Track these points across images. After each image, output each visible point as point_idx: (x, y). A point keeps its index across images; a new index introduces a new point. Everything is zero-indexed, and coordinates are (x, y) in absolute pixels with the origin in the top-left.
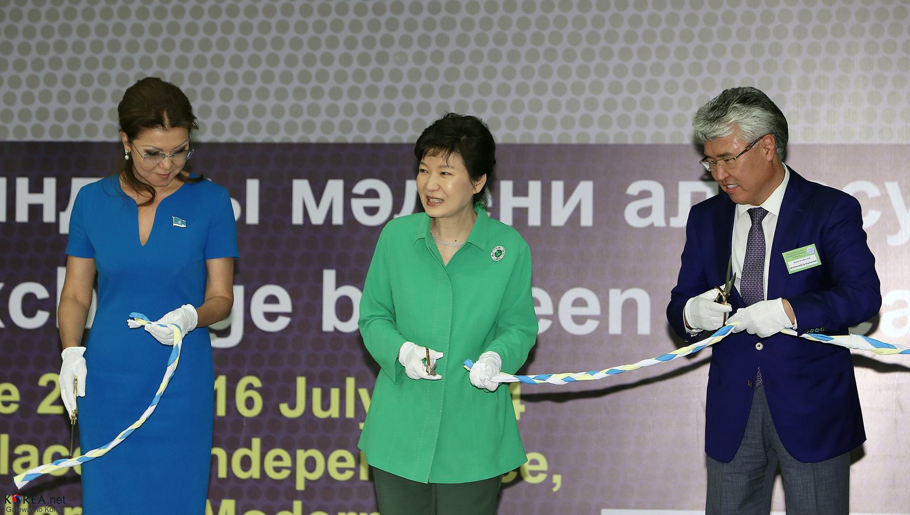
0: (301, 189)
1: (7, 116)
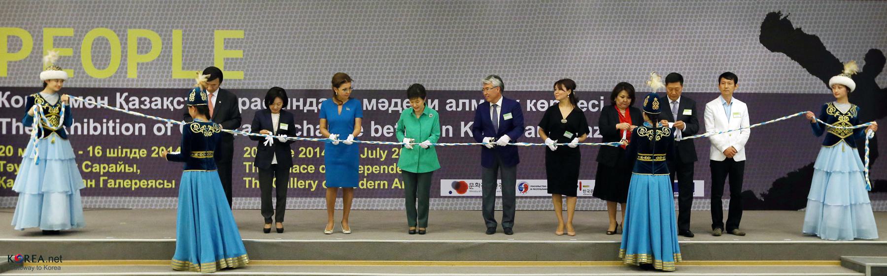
0: (365, 101)
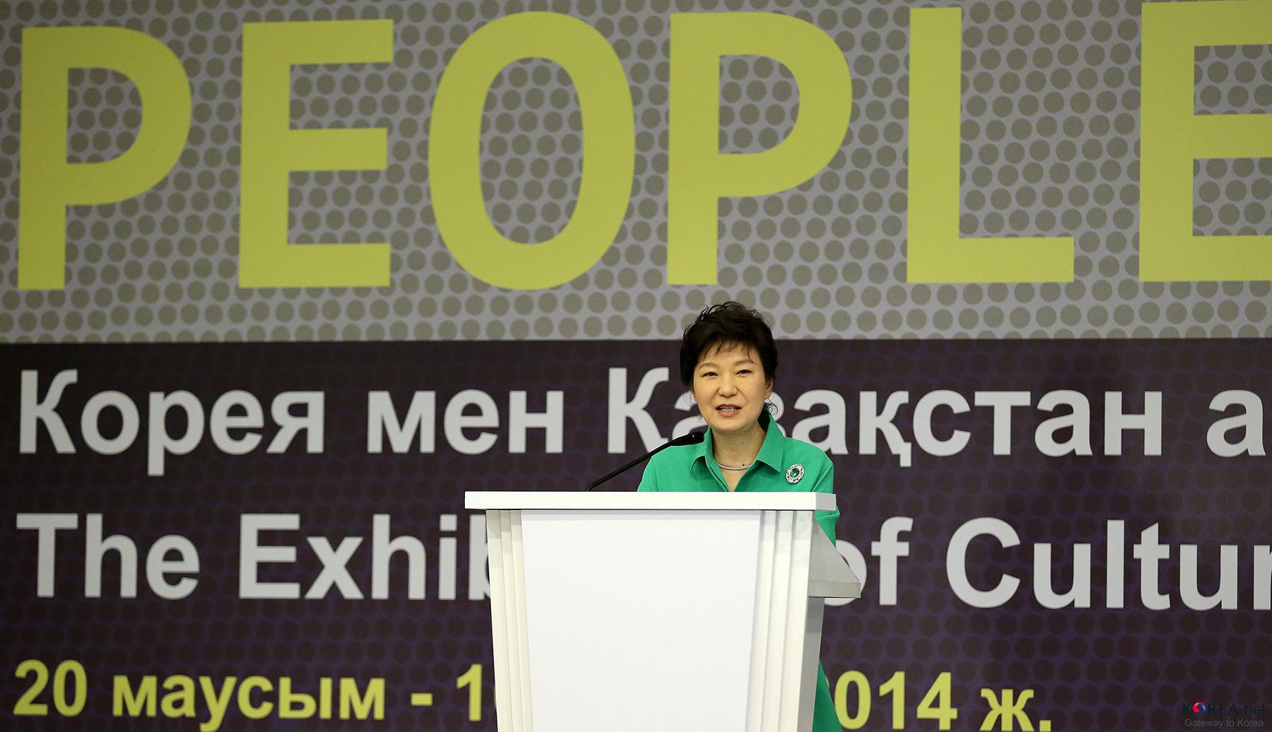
0: (380, 404)
1: (5, 322)
